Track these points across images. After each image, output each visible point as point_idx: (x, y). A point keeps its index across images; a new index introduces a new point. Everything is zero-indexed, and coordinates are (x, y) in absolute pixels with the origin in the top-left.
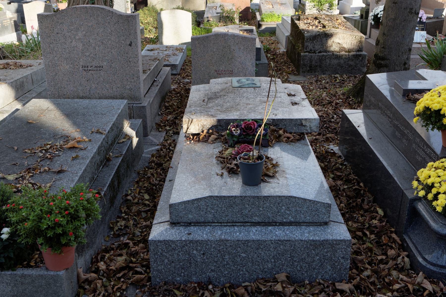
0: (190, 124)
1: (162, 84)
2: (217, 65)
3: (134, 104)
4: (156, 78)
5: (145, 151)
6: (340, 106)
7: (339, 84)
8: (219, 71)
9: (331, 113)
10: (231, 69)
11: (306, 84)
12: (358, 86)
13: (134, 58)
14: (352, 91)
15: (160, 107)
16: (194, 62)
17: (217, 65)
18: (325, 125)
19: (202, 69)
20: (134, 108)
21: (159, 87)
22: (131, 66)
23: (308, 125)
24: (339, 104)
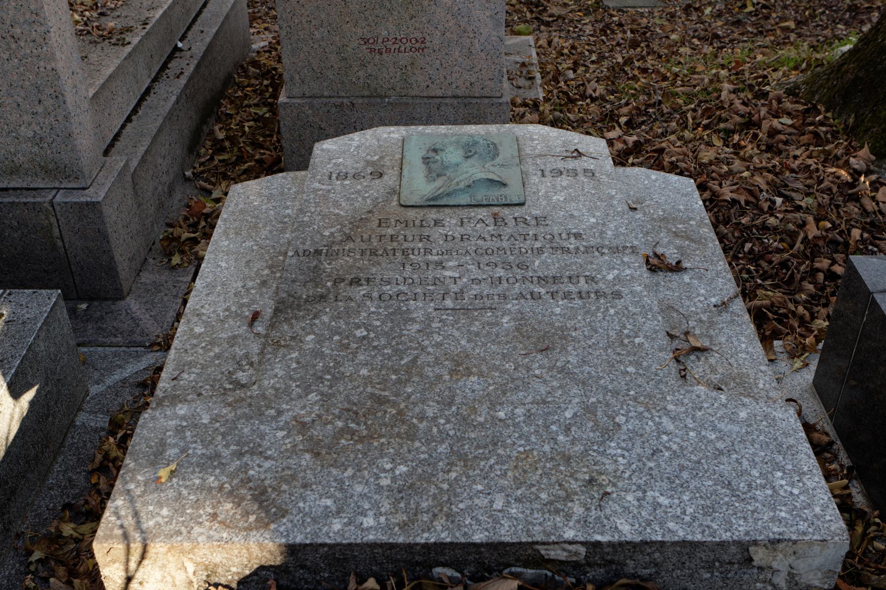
0: (140, 563)
1: (198, 66)
2: (366, 19)
3: (59, 189)
4: (181, 40)
5: (94, 390)
6: (786, 143)
7: (754, 19)
8: (375, 42)
9: (764, 187)
10: (418, 35)
11: (658, 21)
12: (847, 72)
13: (30, 24)
14: (821, 86)
15: (193, 147)
16: (284, 9)
17: (366, 19)
18: (748, 246)
19: (318, 35)
20: (58, 208)
21: (183, 81)
22: (25, 57)
23: (780, 563)
24: (779, 132)
